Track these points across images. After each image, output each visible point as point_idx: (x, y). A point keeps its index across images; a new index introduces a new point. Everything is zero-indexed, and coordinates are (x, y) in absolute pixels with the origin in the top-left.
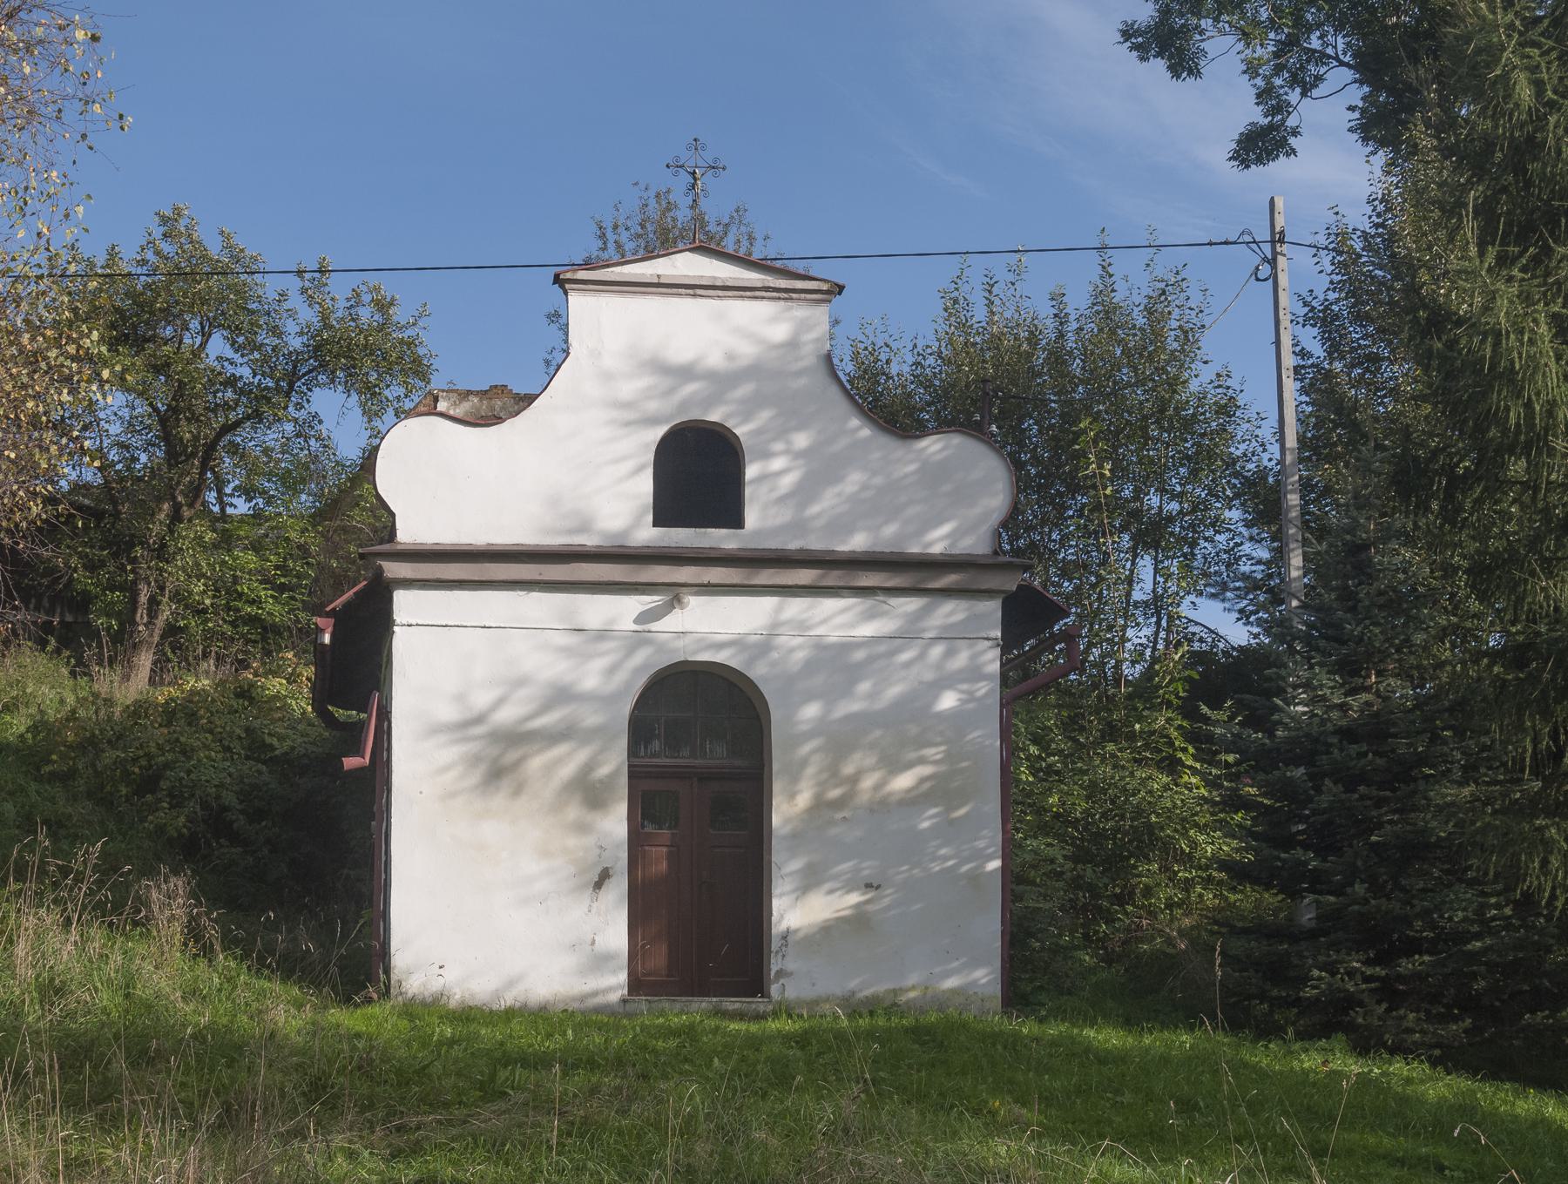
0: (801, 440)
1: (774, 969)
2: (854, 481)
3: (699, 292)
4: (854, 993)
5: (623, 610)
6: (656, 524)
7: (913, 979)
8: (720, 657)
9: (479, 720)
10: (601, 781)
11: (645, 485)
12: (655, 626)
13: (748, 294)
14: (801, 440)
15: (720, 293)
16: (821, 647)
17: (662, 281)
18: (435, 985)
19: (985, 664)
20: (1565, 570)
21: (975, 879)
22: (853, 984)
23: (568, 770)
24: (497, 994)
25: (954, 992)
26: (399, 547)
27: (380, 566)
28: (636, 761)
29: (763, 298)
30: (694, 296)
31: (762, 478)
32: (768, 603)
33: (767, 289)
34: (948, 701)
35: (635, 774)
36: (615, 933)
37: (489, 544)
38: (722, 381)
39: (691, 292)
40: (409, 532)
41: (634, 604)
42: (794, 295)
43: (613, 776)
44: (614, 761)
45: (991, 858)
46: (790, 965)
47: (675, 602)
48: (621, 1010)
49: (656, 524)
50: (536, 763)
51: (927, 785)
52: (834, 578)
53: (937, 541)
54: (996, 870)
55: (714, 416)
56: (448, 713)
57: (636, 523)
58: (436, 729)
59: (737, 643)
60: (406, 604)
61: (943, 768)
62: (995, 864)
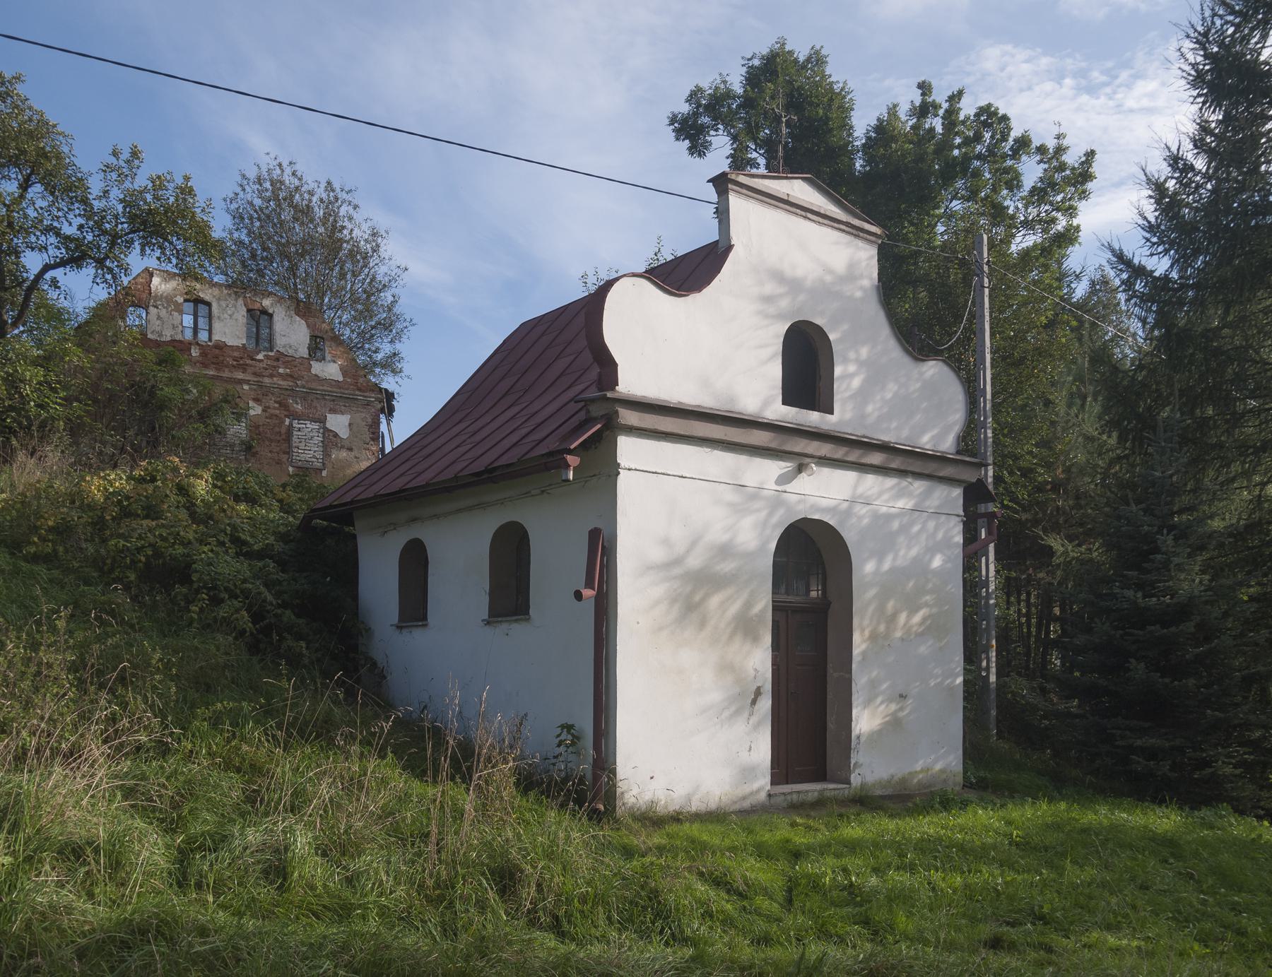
0: (864, 352)
1: (853, 761)
2: (891, 389)
3: (809, 215)
4: (893, 776)
5: (766, 472)
7: (918, 767)
8: (826, 519)
9: (678, 561)
10: (756, 615)
11: (775, 371)
12: (788, 487)
13: (836, 225)
14: (864, 352)
15: (821, 220)
16: (876, 517)
18: (647, 797)
19: (953, 537)
20: (1268, 162)
22: (892, 771)
23: (734, 608)
24: (689, 799)
25: (942, 771)
26: (617, 394)
27: (617, 412)
28: (783, 598)
30: (805, 217)
31: (843, 377)
32: (851, 476)
33: (847, 224)
34: (937, 562)
35: (777, 608)
36: (761, 750)
37: (680, 403)
38: (823, 292)
40: (631, 382)
41: (776, 468)
42: (861, 234)
43: (763, 611)
44: (763, 603)
45: (957, 676)
46: (861, 760)
47: (800, 469)
48: (768, 804)
49: (784, 403)
50: (714, 601)
52: (917, 466)
53: (926, 441)
54: (960, 683)
55: (818, 321)
56: (657, 554)
57: (767, 403)
59: (832, 510)
60: (629, 450)
61: (935, 610)
62: (960, 680)
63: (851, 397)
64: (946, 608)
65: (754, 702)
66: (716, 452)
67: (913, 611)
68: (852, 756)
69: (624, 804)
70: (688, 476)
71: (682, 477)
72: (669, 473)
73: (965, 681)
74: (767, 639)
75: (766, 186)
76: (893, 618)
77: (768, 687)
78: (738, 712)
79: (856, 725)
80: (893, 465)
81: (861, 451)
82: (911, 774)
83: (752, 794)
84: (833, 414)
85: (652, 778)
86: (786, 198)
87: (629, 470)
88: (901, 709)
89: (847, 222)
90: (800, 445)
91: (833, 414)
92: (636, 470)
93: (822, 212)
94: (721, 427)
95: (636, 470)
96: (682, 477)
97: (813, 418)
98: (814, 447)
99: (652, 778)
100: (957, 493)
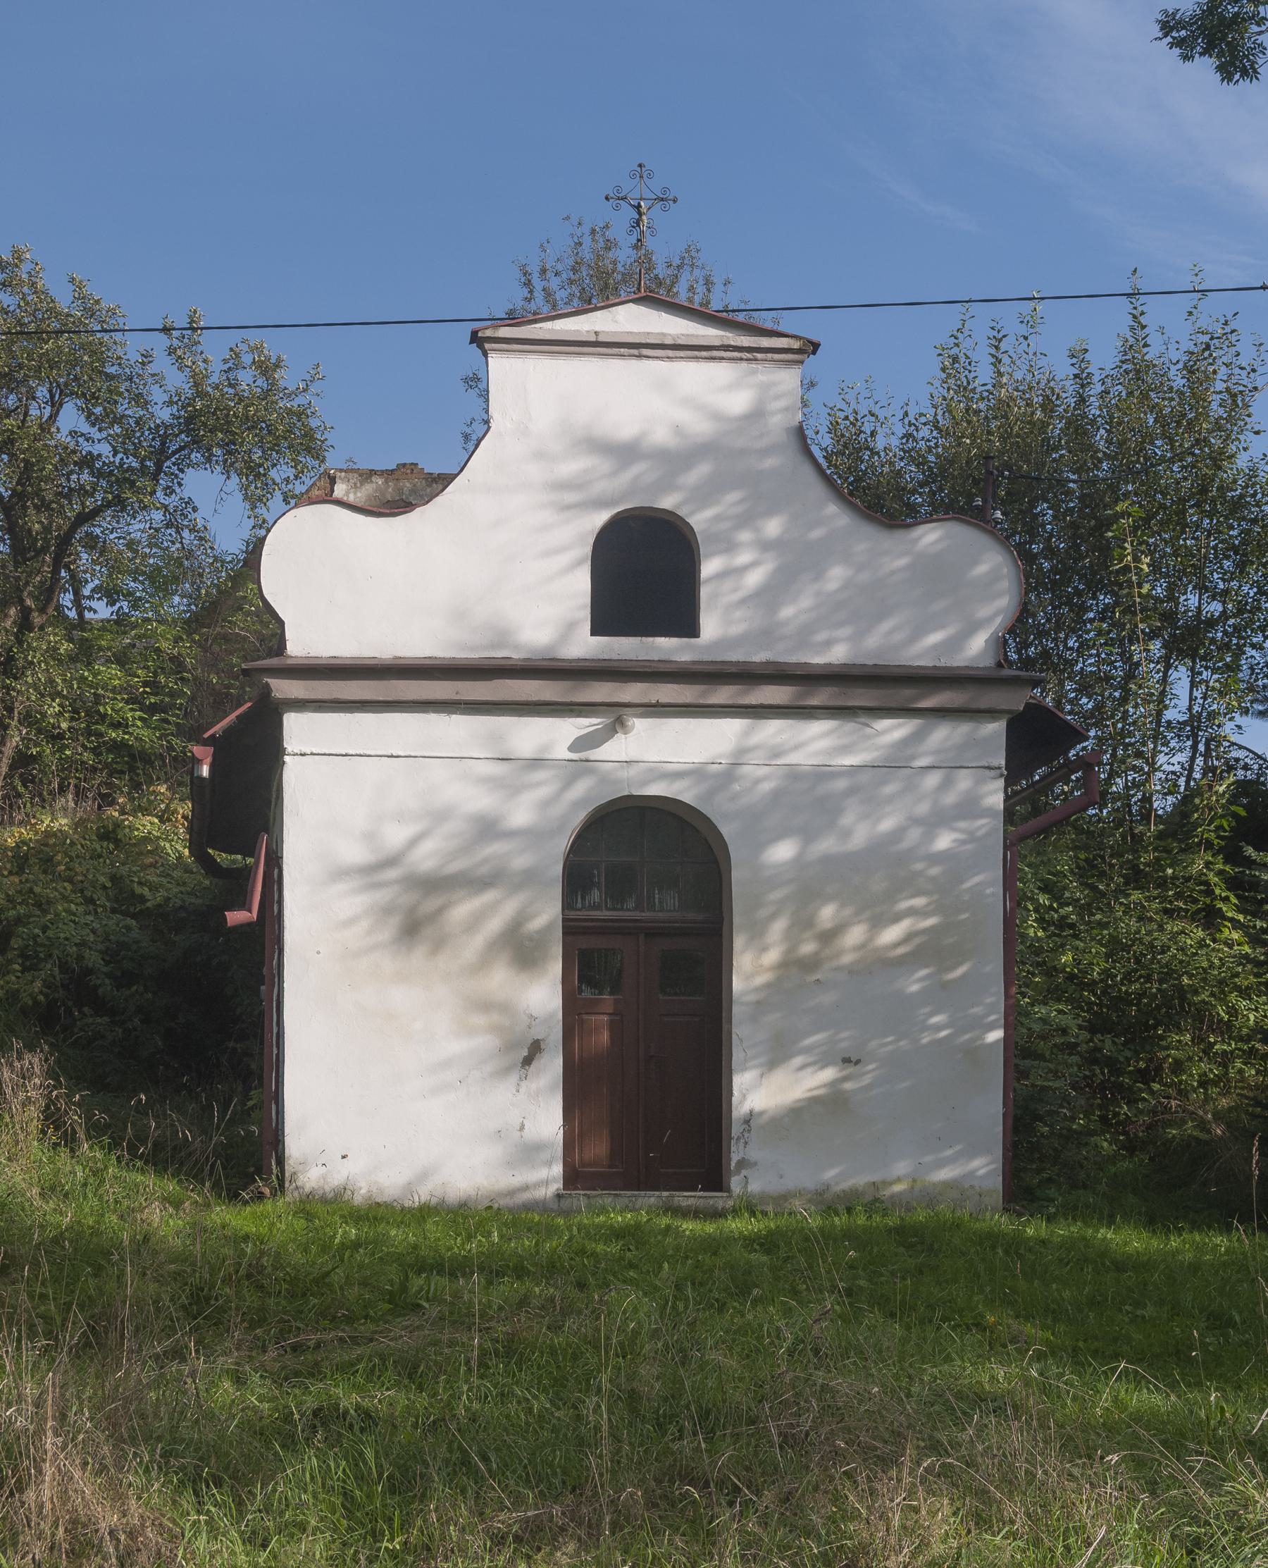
0: (773, 527)
1: (735, 1158)
3: (645, 352)
4: (828, 1187)
6: (595, 632)
9: (391, 861)
11: (581, 582)
13: (704, 354)
15: (670, 353)
17: (601, 339)
21: (974, 1053)
22: (830, 1174)
24: (409, 1188)
26: (289, 662)
27: (267, 685)
28: (572, 914)
29: (722, 358)
30: (640, 356)
33: (697, 358)
39: (635, 352)
41: (569, 729)
42: (759, 356)
43: (549, 928)
45: (991, 1027)
47: (618, 726)
49: (595, 632)
51: (917, 941)
58: (341, 873)
59: (696, 773)
62: (996, 1035)
63: (744, 601)
64: (964, 916)
65: (528, 1061)
66: (454, 716)
67: (879, 922)
68: (733, 1149)
69: (297, 1188)
70: (402, 754)
71: (392, 756)
72: (368, 753)
73: (1006, 1039)
74: (555, 968)
75: (561, 331)
76: (829, 937)
77: (555, 1035)
78: (507, 1071)
79: (741, 1102)
80: (814, 701)
81: (703, 687)
82: (887, 1184)
83: (526, 1188)
84: (592, 634)
85: (344, 1157)
86: (593, 338)
87: (301, 755)
88: (845, 1079)
89: (722, 346)
90: (600, 692)
91: (592, 634)
92: (312, 754)
93: (668, 341)
94: (675, 686)
95: (312, 754)
96: (392, 756)
97: (665, 647)
98: (632, 692)
99: (344, 1157)
100: (996, 729)
